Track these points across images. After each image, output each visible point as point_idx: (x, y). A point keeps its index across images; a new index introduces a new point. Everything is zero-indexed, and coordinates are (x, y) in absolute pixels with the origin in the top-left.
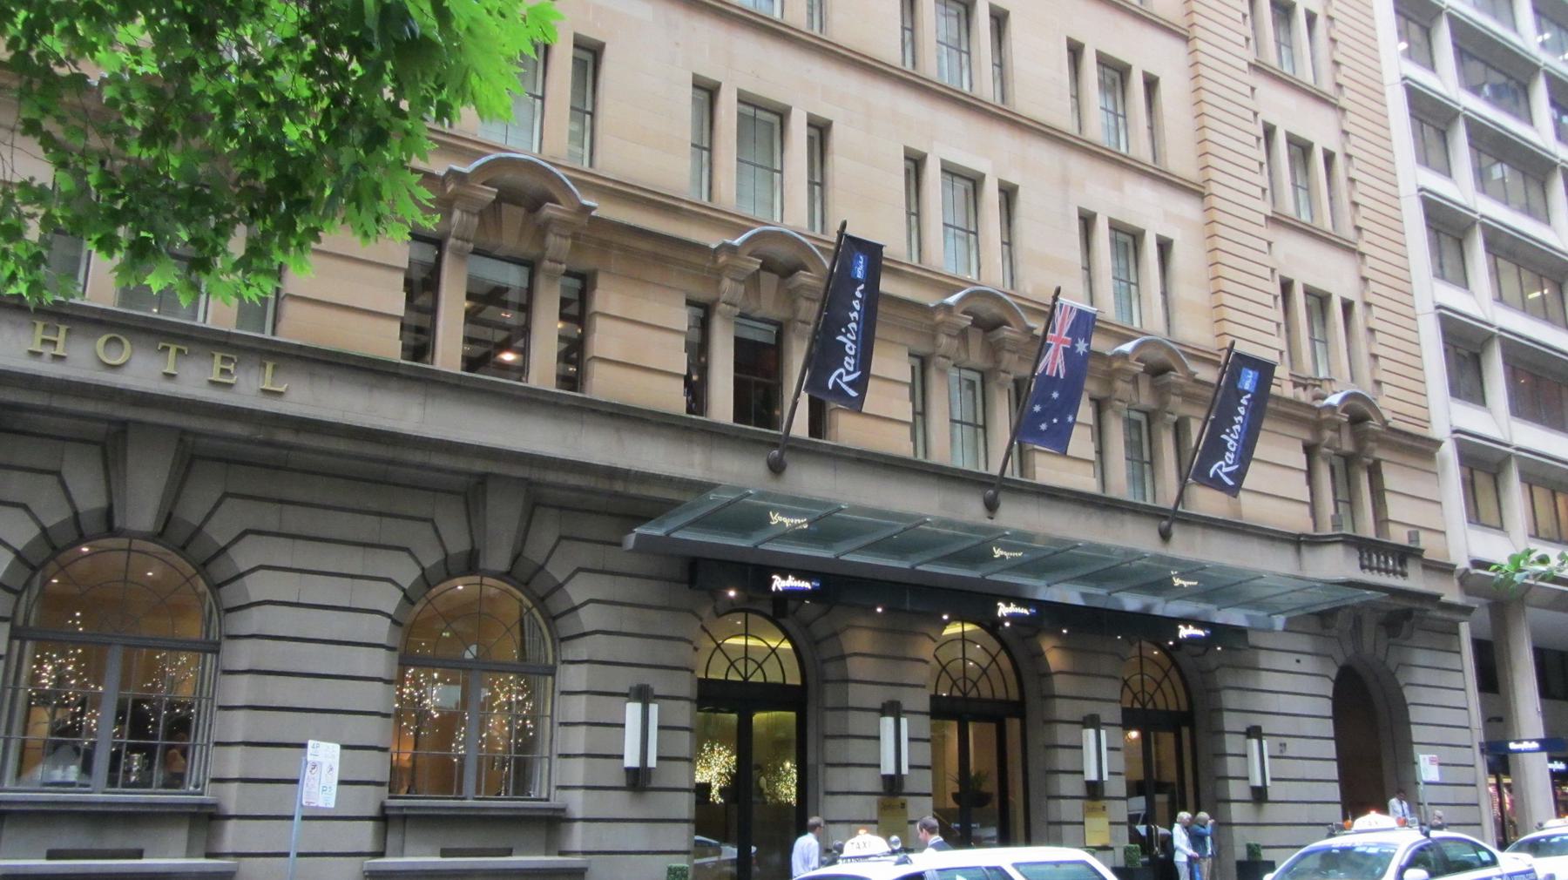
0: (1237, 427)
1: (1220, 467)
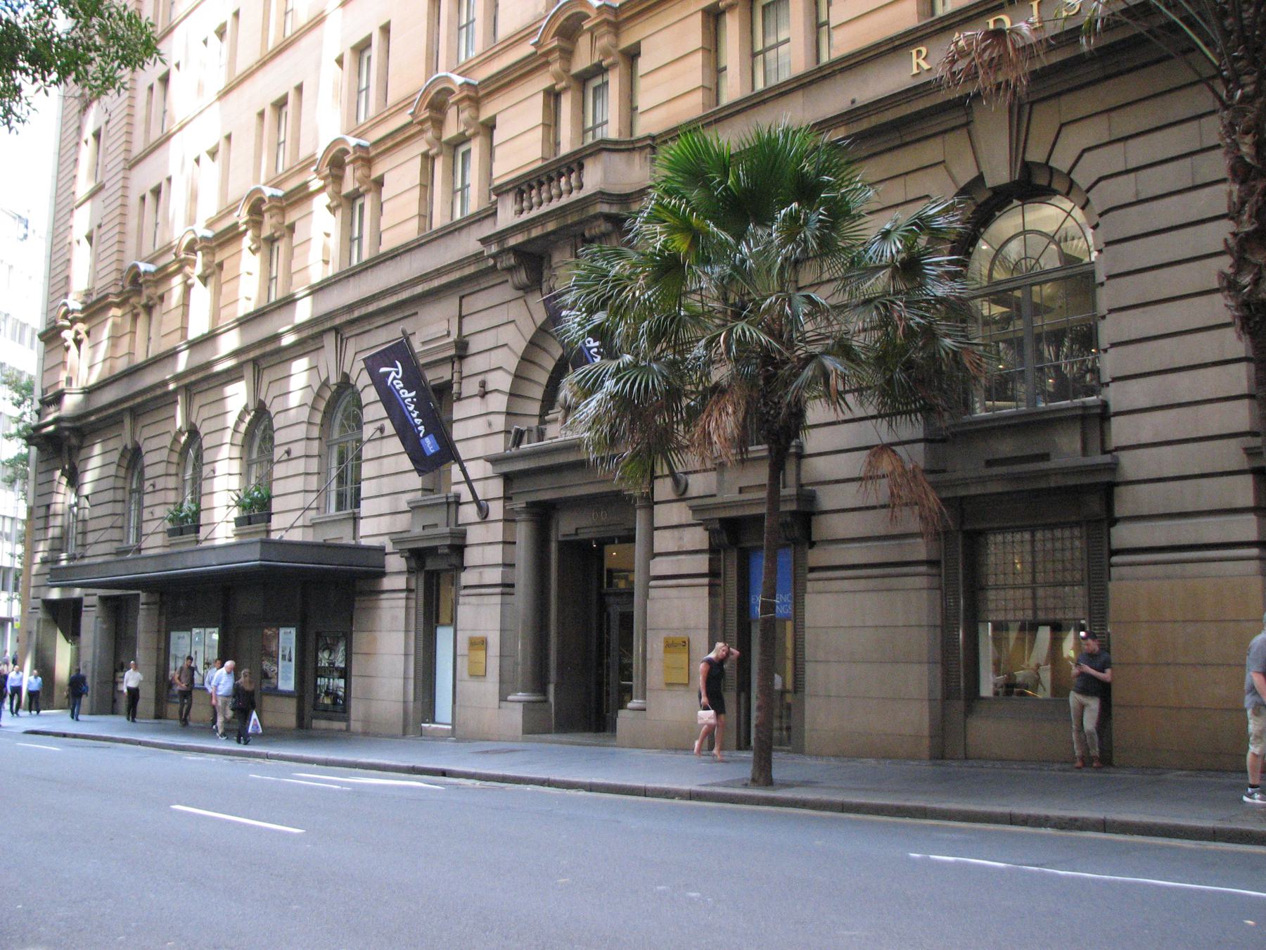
0: (412, 408)
1: (397, 373)
